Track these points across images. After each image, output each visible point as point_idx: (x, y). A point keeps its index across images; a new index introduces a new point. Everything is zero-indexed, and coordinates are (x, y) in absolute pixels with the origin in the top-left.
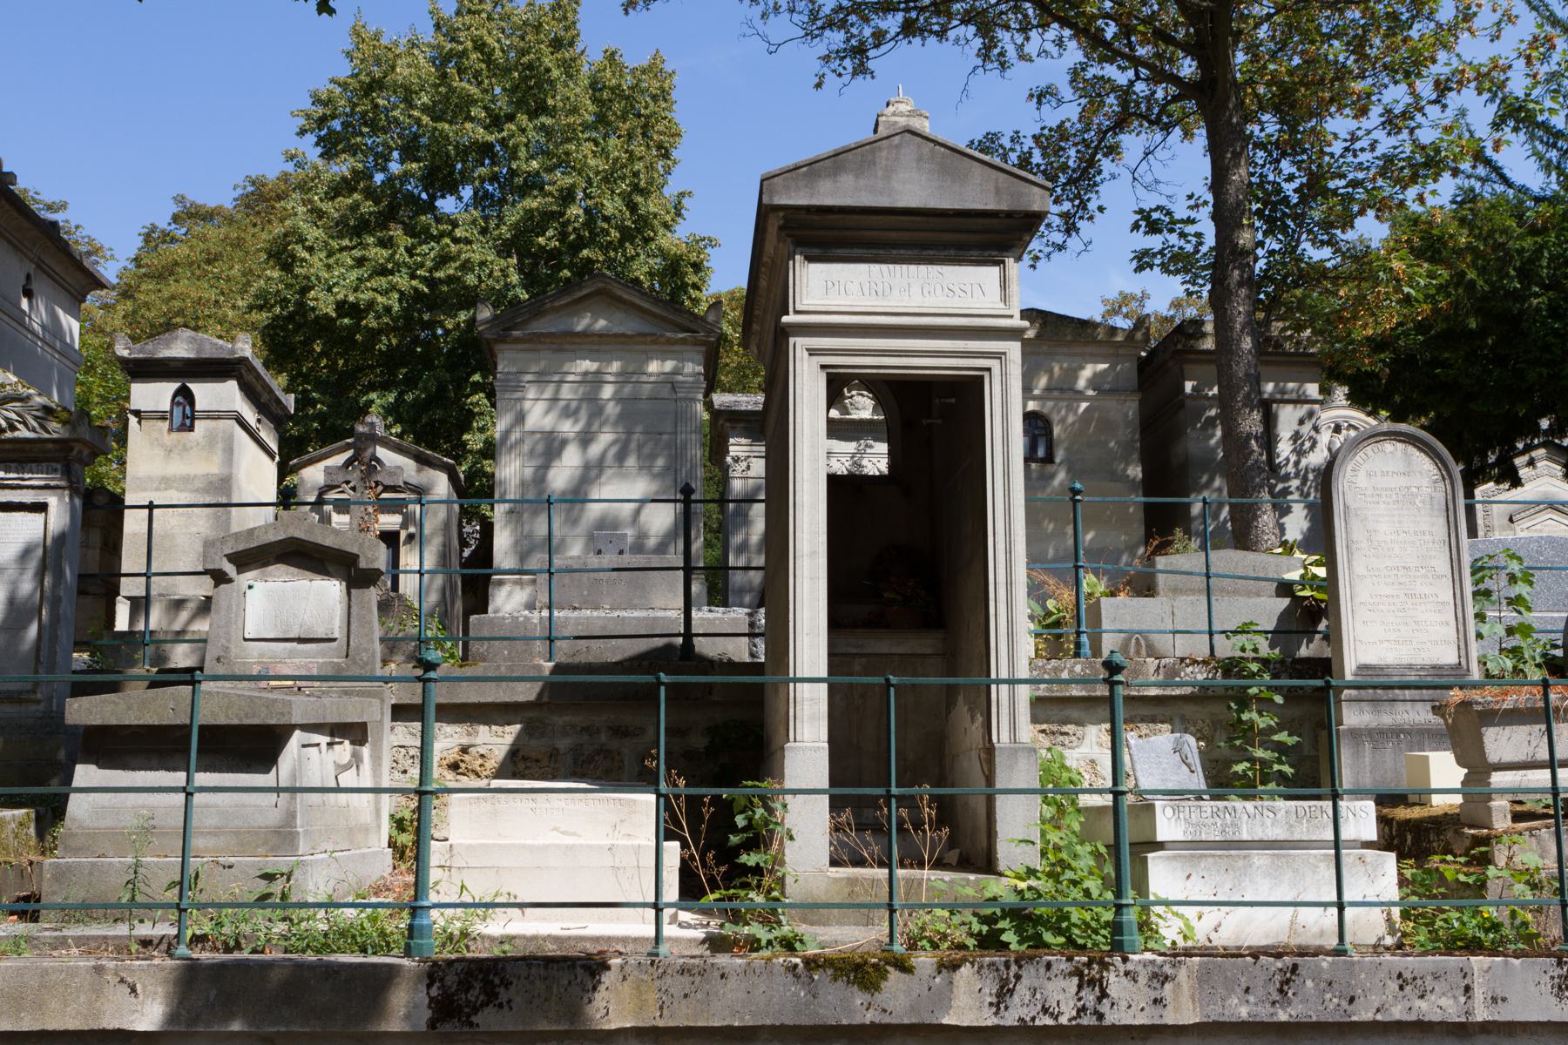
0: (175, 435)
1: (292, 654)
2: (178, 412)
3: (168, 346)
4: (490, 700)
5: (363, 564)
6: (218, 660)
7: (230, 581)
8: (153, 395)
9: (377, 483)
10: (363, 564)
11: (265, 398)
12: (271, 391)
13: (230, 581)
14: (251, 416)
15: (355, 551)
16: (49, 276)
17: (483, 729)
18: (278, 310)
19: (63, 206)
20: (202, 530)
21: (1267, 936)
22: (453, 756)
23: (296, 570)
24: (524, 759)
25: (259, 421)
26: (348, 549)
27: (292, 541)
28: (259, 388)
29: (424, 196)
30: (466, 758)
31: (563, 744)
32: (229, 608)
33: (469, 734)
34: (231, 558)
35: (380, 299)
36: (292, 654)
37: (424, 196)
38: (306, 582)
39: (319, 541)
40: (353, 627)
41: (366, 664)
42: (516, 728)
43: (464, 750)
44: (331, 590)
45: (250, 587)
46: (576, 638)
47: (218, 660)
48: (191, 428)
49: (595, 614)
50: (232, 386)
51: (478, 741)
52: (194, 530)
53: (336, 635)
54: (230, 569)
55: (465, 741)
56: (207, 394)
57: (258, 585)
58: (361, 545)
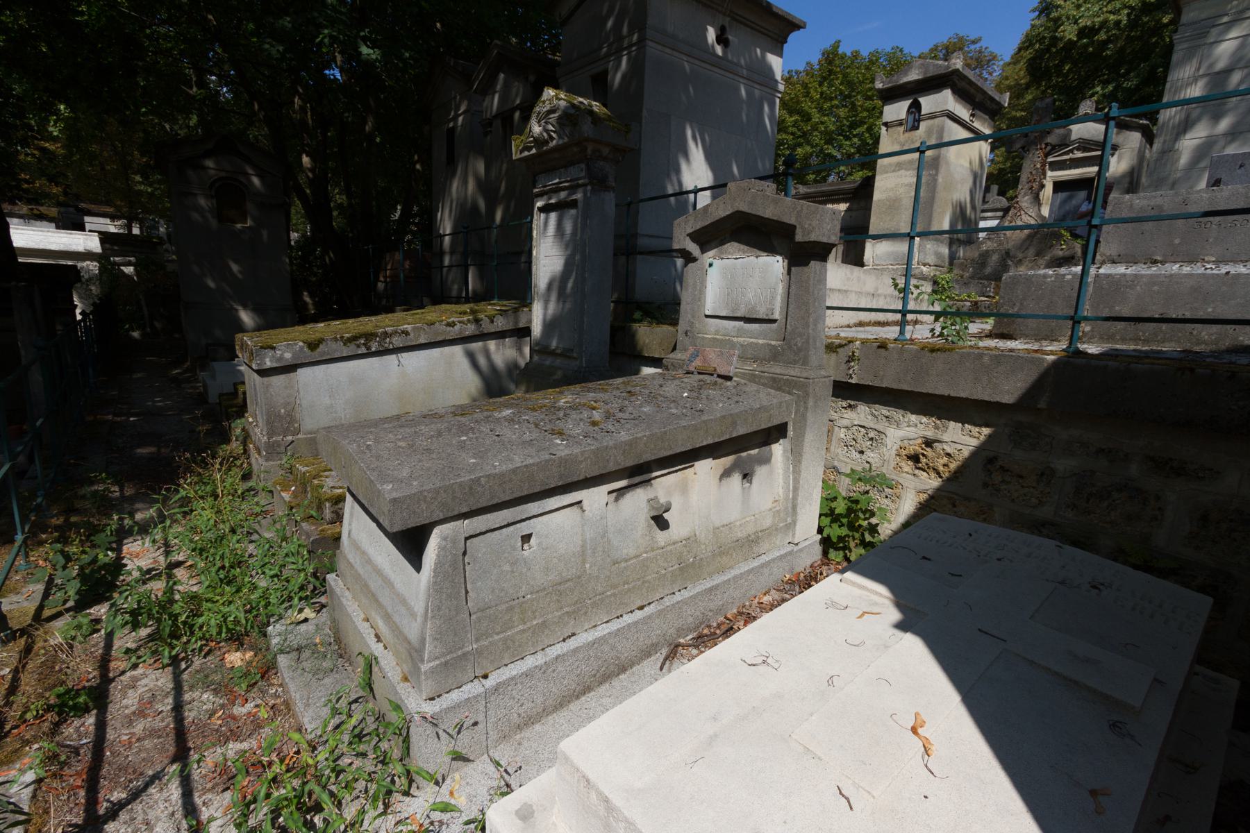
0: (907, 135)
1: (740, 333)
2: (911, 118)
3: (906, 74)
4: (963, 395)
5: (799, 237)
7: (694, 260)
8: (897, 110)
9: (1047, 144)
10: (799, 237)
11: (979, 98)
12: (984, 93)
13: (694, 260)
14: (963, 112)
15: (792, 221)
16: (741, 23)
18: (1037, 46)
19: (980, 39)
22: (915, 447)
24: (1003, 469)
25: (972, 115)
26: (786, 220)
27: (738, 215)
28: (972, 91)
30: (929, 452)
31: (1062, 465)
33: (937, 428)
34: (694, 237)
35: (1112, 17)
36: (740, 333)
39: (760, 213)
41: (800, 350)
42: (986, 431)
44: (776, 265)
46: (1107, 319)
48: (917, 128)
49: (1187, 269)
50: (947, 93)
51: (946, 437)
53: (777, 316)
54: (693, 248)
55: (930, 434)
56: (928, 103)
57: (716, 262)
58: (799, 215)
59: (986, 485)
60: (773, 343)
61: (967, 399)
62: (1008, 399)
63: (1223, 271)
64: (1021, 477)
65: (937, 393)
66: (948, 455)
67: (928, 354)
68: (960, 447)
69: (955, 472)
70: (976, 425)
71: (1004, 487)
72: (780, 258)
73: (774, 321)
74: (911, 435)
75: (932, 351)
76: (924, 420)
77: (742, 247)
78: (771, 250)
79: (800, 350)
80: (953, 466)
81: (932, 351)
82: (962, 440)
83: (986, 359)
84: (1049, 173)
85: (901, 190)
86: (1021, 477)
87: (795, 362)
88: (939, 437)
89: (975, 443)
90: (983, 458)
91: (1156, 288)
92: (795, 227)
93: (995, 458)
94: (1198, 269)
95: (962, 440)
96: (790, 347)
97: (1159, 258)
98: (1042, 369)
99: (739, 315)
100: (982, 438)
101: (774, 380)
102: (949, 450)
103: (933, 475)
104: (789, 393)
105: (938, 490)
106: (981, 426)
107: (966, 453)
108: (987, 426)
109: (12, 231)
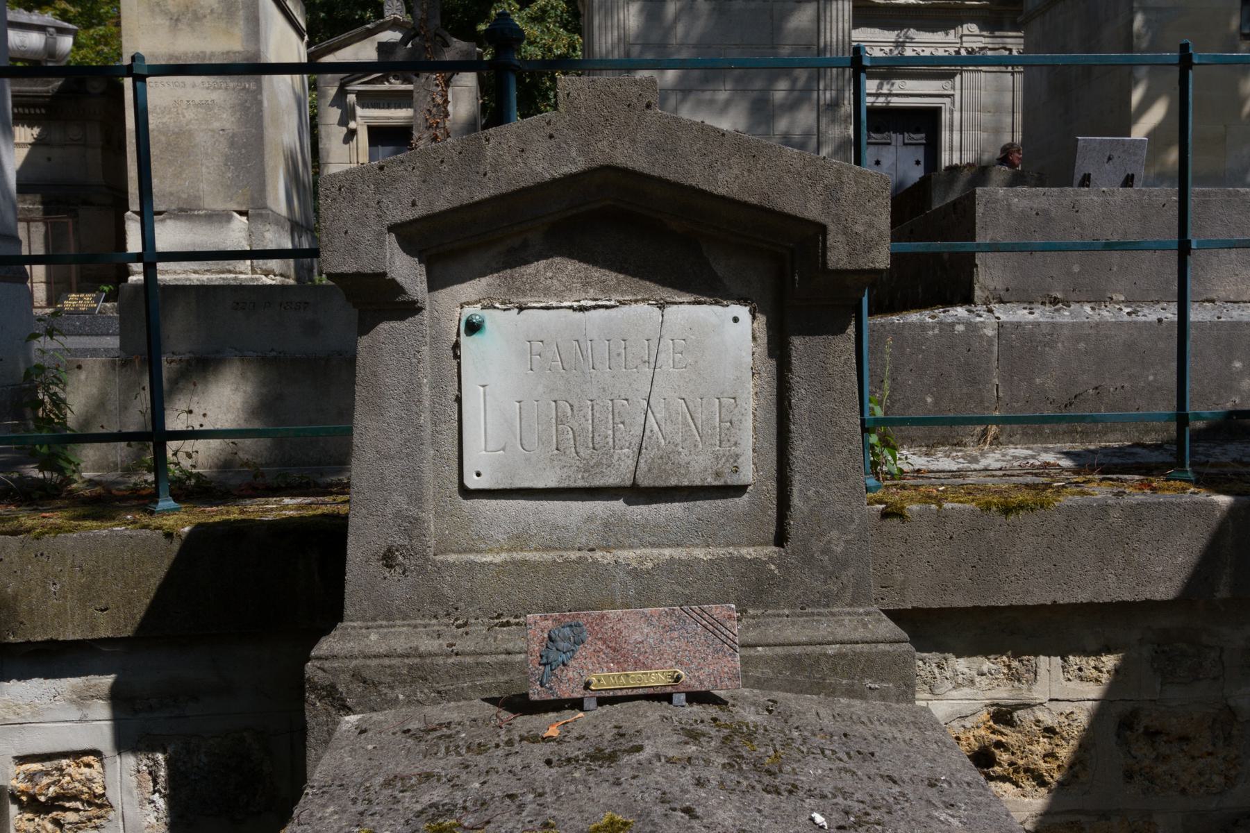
1: (611, 536)
4: (1083, 597)
6: (388, 559)
7: (411, 309)
13: (411, 309)
15: (813, 211)
17: (1047, 664)
20: (227, 126)
21: (193, 57)
22: (979, 732)
23: (612, 277)
24: (1152, 735)
26: (791, 204)
29: (482, 27)
30: (1011, 737)
32: (412, 395)
33: (1014, 677)
34: (413, 236)
36: (611, 536)
37: (482, 27)
38: (644, 312)
40: (800, 450)
41: (842, 563)
42: (1110, 661)
43: (1003, 715)
44: (729, 333)
45: (473, 328)
47: (388, 559)
51: (1039, 692)
52: (216, 125)
53: (747, 475)
54: (406, 270)
55: (1004, 694)
57: (496, 320)
58: (831, 195)
59: (1129, 776)
60: (748, 552)
61: (1090, 605)
62: (1165, 591)
63: (1153, 317)
64: (1184, 739)
65: (1030, 601)
66: (1050, 731)
67: (999, 519)
68: (1068, 707)
69: (1071, 766)
70: (1086, 653)
71: (1161, 768)
72: (743, 312)
73: (740, 490)
74: (966, 707)
75: (1007, 510)
76: (986, 665)
77: (597, 273)
78: (710, 288)
79: (842, 563)
80: (1065, 753)
81: (1007, 510)
82: (1067, 691)
83: (1115, 514)
84: (359, 111)
85: (190, 114)
86: (1184, 739)
87: (827, 599)
88: (1026, 695)
89: (1094, 691)
90: (1116, 719)
91: (1082, 345)
92: (822, 229)
93: (1135, 714)
94: (1107, 314)
95: (1067, 691)
96: (809, 561)
97: (1059, 296)
98: (1214, 524)
99: (611, 480)
100: (1105, 678)
101: (796, 663)
102: (1048, 720)
103: (1028, 785)
104: (851, 693)
105: (1047, 814)
106: (1097, 653)
107: (1083, 719)
108: (1109, 651)
109: (156, 225)
